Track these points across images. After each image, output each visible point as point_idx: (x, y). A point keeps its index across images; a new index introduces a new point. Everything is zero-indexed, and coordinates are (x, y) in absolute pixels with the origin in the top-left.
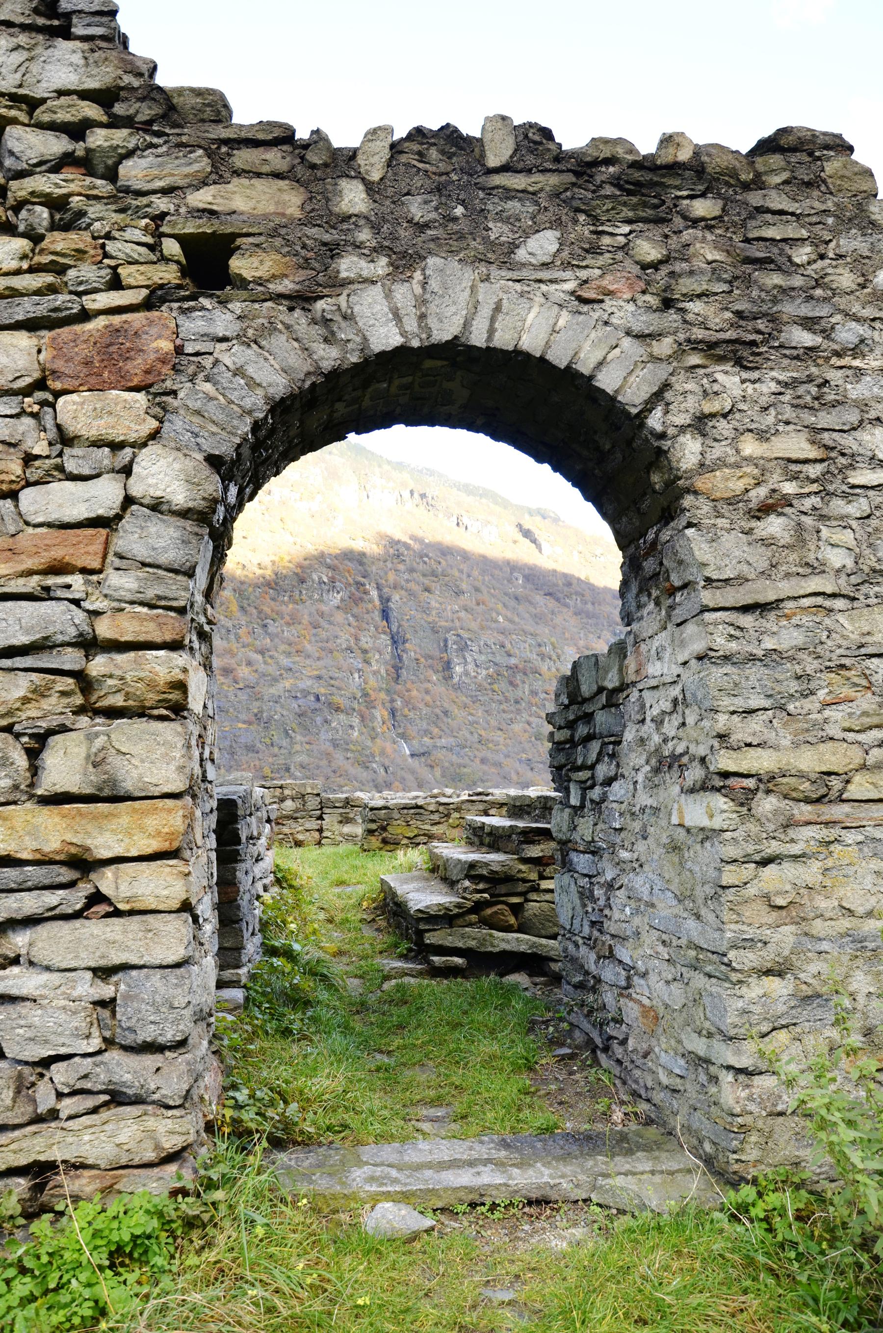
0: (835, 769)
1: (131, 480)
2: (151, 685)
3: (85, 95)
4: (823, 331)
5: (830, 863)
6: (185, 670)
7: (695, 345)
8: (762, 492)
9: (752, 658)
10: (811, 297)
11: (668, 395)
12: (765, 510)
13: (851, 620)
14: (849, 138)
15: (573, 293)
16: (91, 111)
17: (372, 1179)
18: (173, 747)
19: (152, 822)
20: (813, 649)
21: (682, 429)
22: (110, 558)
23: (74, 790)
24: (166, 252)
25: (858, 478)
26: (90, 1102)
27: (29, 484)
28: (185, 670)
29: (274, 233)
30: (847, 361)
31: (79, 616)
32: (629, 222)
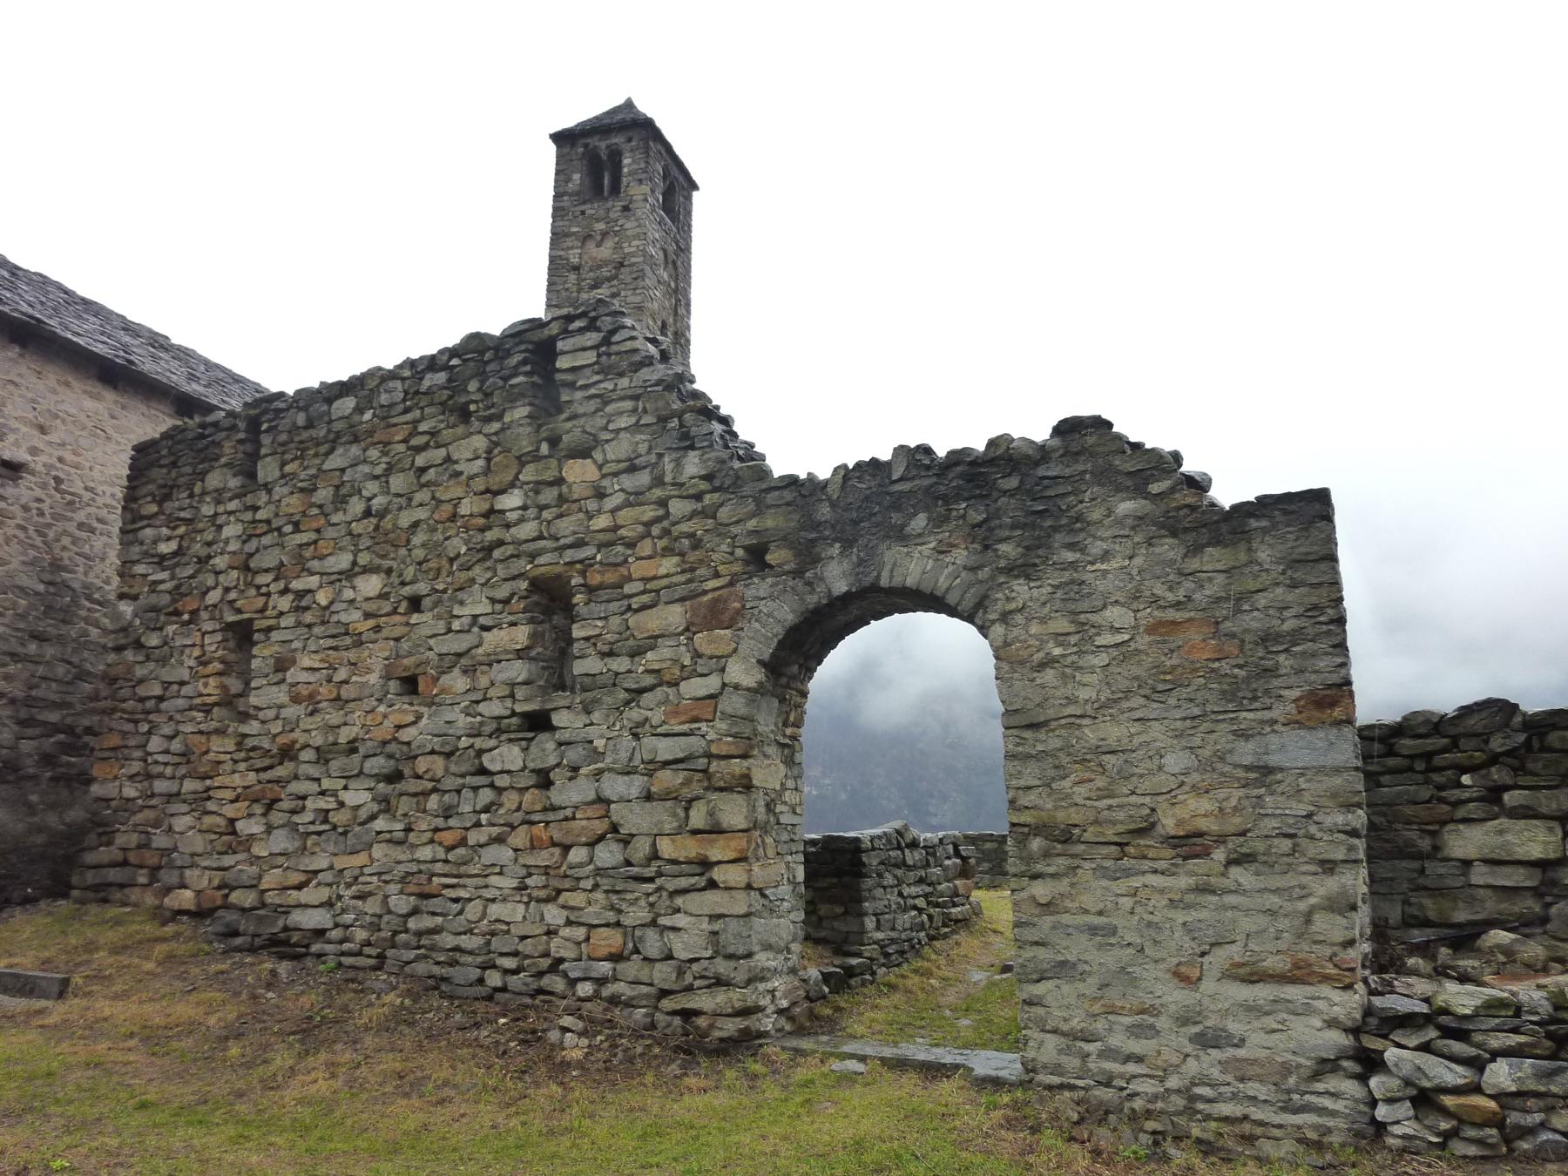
2: (733, 776)
5: (1075, 880)
6: (749, 769)
7: (1001, 571)
8: (1041, 655)
9: (1029, 757)
10: (1072, 530)
11: (986, 603)
12: (1042, 666)
13: (1093, 731)
15: (934, 549)
16: (704, 486)
19: (733, 844)
20: (1066, 748)
22: (718, 714)
23: (701, 827)
25: (1100, 641)
26: (706, 982)
28: (749, 769)
29: (784, 539)
30: (1098, 566)
31: (703, 743)
32: (966, 499)
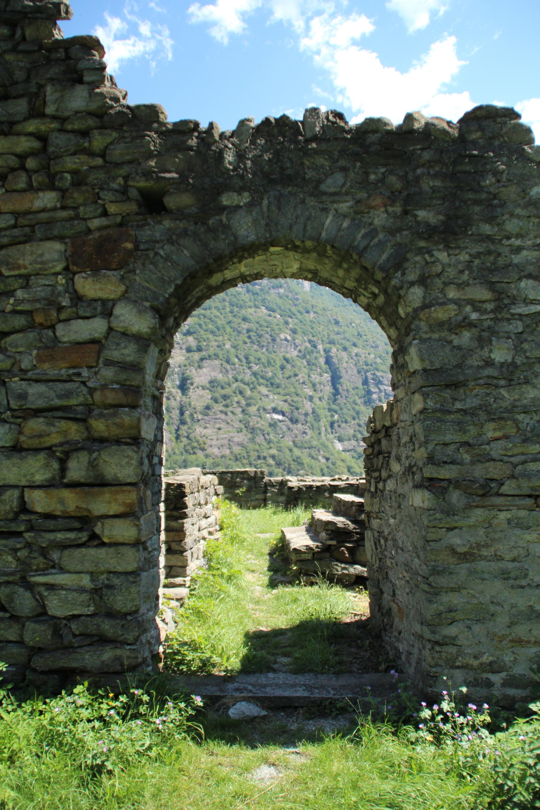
0: (495, 477)
1: (112, 318)
3: (90, 114)
4: (498, 225)
17: (237, 690)
18: (132, 458)
19: (121, 498)
21: (412, 284)
23: (82, 480)
24: (130, 195)
27: (60, 321)
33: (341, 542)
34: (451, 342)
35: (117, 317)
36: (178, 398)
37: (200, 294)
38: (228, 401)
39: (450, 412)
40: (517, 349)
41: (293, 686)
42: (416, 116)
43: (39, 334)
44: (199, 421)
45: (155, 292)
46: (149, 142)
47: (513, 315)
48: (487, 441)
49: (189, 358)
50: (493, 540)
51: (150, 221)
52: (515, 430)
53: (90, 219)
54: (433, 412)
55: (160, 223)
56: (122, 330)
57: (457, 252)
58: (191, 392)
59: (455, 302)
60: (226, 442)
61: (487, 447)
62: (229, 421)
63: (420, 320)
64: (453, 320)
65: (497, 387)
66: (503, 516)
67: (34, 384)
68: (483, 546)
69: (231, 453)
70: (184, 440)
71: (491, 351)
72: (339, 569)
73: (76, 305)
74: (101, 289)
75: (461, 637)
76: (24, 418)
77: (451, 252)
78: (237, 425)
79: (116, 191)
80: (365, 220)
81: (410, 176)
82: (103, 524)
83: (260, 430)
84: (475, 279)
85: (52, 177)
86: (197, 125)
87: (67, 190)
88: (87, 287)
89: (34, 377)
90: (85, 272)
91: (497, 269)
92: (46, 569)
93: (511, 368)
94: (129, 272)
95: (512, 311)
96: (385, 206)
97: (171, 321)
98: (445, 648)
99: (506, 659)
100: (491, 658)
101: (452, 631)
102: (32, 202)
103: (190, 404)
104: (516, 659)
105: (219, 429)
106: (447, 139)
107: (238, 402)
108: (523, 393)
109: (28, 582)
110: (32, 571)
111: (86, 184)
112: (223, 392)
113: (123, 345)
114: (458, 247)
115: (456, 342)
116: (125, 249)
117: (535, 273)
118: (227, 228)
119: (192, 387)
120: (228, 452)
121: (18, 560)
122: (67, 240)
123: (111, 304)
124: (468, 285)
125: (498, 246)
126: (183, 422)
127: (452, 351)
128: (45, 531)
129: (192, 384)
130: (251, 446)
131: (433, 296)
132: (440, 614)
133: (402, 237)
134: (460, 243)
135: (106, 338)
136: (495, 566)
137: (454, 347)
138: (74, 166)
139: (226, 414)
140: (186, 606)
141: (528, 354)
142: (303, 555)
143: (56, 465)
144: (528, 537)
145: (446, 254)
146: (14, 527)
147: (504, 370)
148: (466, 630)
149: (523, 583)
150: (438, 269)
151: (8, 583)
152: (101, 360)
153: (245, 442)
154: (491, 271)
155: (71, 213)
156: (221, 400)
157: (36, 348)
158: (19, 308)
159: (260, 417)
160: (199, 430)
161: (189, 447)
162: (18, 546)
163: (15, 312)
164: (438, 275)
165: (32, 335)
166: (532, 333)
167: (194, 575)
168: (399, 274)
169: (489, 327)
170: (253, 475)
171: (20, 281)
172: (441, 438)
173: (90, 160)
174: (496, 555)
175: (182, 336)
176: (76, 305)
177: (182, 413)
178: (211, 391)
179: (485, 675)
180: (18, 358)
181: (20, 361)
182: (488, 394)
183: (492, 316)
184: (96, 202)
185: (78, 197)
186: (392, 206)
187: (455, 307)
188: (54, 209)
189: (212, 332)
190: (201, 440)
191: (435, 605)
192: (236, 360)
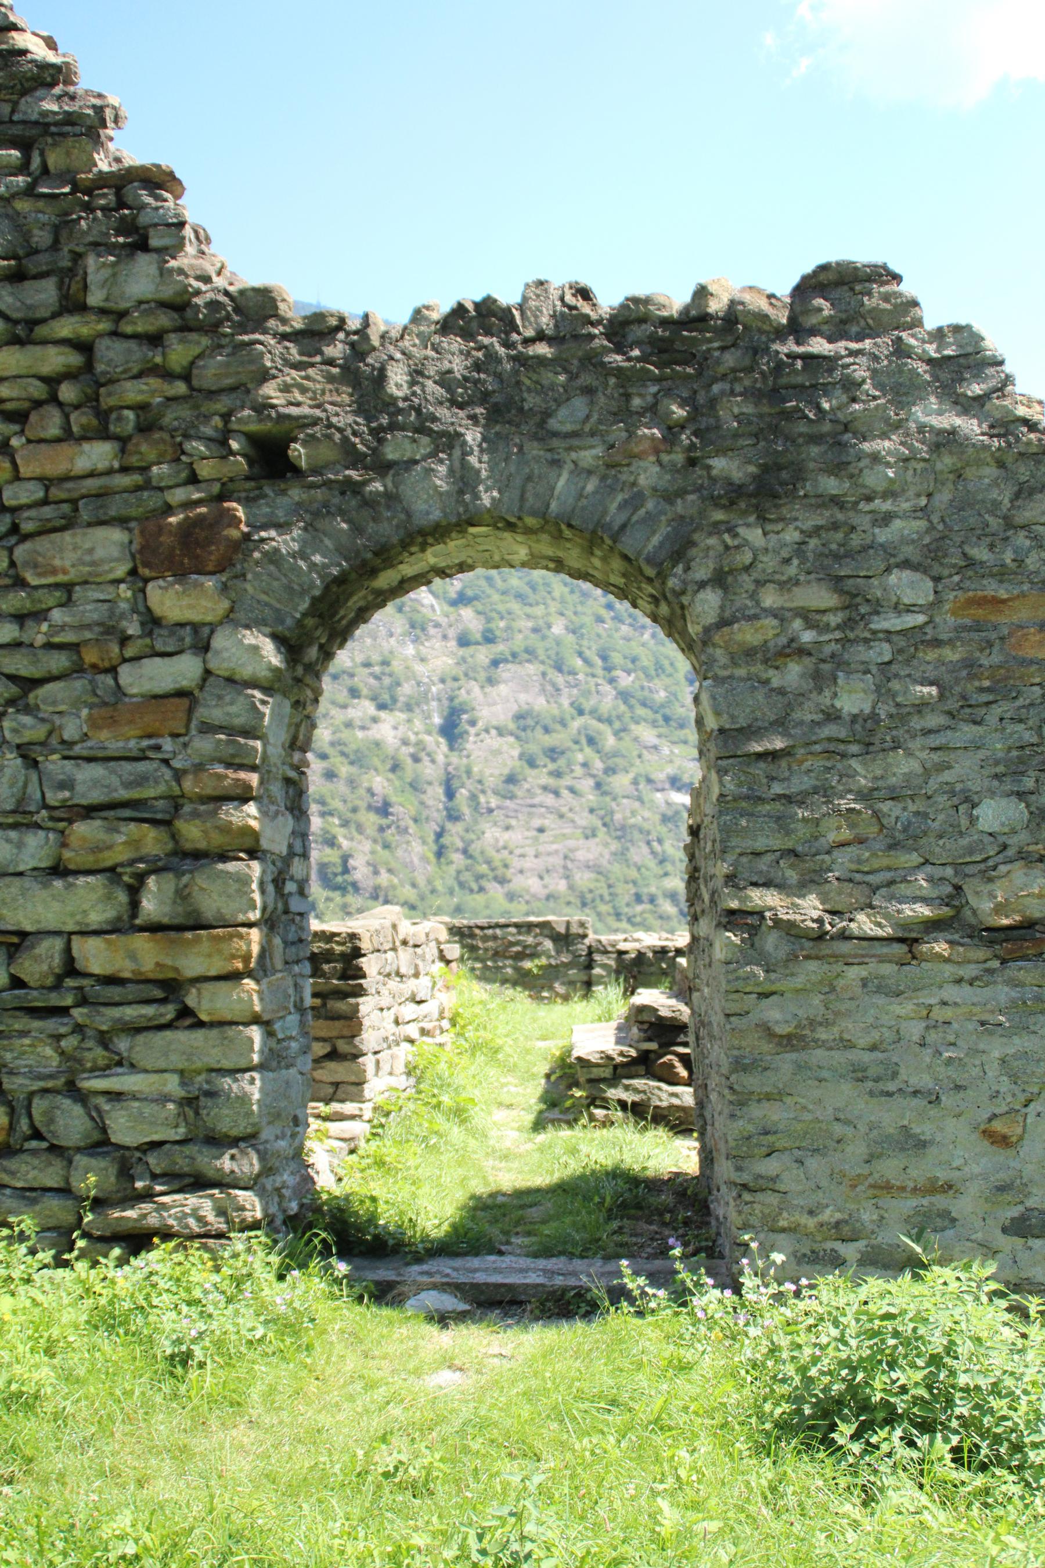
1: (209, 655)
4: (851, 476)
13: (864, 764)
14: (894, 267)
21: (702, 585)
23: (166, 920)
27: (125, 660)
33: (666, 1045)
34: (766, 682)
35: (217, 653)
36: (440, 758)
37: (362, 603)
38: (562, 762)
39: (760, 799)
40: (881, 691)
41: (521, 1271)
42: (711, 288)
43: (91, 682)
44: (490, 811)
45: (278, 610)
46: (262, 354)
47: (874, 632)
48: (827, 847)
49: (464, 660)
50: (837, 1014)
51: (268, 490)
52: (876, 829)
53: (170, 487)
54: (735, 800)
55: (283, 492)
56: (226, 674)
57: (779, 526)
58: (470, 744)
59: (775, 613)
60: (557, 861)
61: (827, 857)
62: (564, 810)
63: (714, 645)
64: (771, 644)
65: (843, 756)
66: (854, 973)
67: (84, 765)
68: (821, 1024)
69: (571, 887)
70: (457, 858)
71: (835, 695)
72: (664, 1096)
73: (150, 634)
74: (191, 607)
75: (785, 1176)
76: (71, 821)
77: (769, 527)
78: (584, 819)
79: (210, 439)
80: (623, 477)
81: (701, 398)
82: (199, 993)
83: (641, 831)
84: (809, 573)
85: (103, 416)
86: (342, 320)
87: (129, 438)
88: (168, 603)
89: (85, 753)
90: (163, 578)
91: (849, 555)
92: (108, 1067)
93: (869, 725)
94: (236, 577)
95: (872, 626)
96: (657, 452)
97: (313, 653)
98: (760, 1196)
99: (866, 1217)
100: (838, 1216)
101: (770, 1167)
102: (72, 460)
103: (469, 773)
104: (882, 1218)
105: (541, 830)
106: (766, 327)
107: (585, 765)
108: (889, 765)
109: (79, 1090)
110: (84, 1071)
111: (161, 428)
112: (548, 740)
113: (228, 699)
114: (782, 519)
115: (775, 683)
116: (227, 539)
117: (916, 559)
118: (391, 498)
119: (472, 731)
120: (562, 886)
121: (62, 1053)
122: (133, 524)
123: (206, 630)
124: (797, 583)
125: (851, 514)
126: (453, 816)
127: (767, 696)
128: (106, 1004)
129: (473, 723)
130: (617, 869)
131: (738, 604)
132: (749, 1138)
133: (688, 505)
134: (784, 511)
135: (201, 688)
136: (839, 1057)
137: (772, 690)
138: (140, 398)
139: (556, 793)
140: (361, 1152)
141: (899, 699)
142: (595, 1070)
143: (122, 897)
144: (898, 1010)
145: (760, 531)
146: (55, 1000)
147: (858, 727)
148: (795, 1165)
149: (891, 1087)
150: (747, 557)
151: (45, 1091)
152: (193, 725)
153: (604, 862)
154: (837, 557)
155: (137, 478)
156: (542, 760)
157: (86, 704)
158: (57, 640)
159: (640, 799)
160: (491, 834)
161: (467, 876)
162: (63, 1030)
163: (49, 646)
164: (747, 569)
165: (78, 685)
166: (908, 662)
167: (380, 1100)
168: (679, 569)
169: (833, 656)
170: (562, 930)
171: (58, 594)
172: (749, 844)
173: (166, 386)
174: (842, 1039)
175: (447, 608)
176: (150, 634)
177: (450, 794)
178: (517, 738)
179: (829, 1245)
180: (58, 722)
181: (61, 727)
182: (828, 769)
183: (838, 635)
184: (178, 460)
185: (146, 449)
186: (669, 453)
187: (775, 622)
188: (109, 472)
189: (520, 597)
190: (497, 858)
191: (741, 1123)
192: (579, 662)
